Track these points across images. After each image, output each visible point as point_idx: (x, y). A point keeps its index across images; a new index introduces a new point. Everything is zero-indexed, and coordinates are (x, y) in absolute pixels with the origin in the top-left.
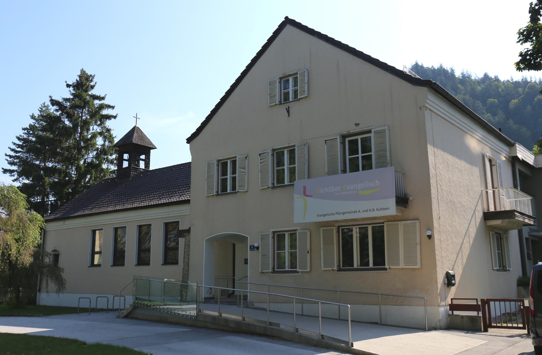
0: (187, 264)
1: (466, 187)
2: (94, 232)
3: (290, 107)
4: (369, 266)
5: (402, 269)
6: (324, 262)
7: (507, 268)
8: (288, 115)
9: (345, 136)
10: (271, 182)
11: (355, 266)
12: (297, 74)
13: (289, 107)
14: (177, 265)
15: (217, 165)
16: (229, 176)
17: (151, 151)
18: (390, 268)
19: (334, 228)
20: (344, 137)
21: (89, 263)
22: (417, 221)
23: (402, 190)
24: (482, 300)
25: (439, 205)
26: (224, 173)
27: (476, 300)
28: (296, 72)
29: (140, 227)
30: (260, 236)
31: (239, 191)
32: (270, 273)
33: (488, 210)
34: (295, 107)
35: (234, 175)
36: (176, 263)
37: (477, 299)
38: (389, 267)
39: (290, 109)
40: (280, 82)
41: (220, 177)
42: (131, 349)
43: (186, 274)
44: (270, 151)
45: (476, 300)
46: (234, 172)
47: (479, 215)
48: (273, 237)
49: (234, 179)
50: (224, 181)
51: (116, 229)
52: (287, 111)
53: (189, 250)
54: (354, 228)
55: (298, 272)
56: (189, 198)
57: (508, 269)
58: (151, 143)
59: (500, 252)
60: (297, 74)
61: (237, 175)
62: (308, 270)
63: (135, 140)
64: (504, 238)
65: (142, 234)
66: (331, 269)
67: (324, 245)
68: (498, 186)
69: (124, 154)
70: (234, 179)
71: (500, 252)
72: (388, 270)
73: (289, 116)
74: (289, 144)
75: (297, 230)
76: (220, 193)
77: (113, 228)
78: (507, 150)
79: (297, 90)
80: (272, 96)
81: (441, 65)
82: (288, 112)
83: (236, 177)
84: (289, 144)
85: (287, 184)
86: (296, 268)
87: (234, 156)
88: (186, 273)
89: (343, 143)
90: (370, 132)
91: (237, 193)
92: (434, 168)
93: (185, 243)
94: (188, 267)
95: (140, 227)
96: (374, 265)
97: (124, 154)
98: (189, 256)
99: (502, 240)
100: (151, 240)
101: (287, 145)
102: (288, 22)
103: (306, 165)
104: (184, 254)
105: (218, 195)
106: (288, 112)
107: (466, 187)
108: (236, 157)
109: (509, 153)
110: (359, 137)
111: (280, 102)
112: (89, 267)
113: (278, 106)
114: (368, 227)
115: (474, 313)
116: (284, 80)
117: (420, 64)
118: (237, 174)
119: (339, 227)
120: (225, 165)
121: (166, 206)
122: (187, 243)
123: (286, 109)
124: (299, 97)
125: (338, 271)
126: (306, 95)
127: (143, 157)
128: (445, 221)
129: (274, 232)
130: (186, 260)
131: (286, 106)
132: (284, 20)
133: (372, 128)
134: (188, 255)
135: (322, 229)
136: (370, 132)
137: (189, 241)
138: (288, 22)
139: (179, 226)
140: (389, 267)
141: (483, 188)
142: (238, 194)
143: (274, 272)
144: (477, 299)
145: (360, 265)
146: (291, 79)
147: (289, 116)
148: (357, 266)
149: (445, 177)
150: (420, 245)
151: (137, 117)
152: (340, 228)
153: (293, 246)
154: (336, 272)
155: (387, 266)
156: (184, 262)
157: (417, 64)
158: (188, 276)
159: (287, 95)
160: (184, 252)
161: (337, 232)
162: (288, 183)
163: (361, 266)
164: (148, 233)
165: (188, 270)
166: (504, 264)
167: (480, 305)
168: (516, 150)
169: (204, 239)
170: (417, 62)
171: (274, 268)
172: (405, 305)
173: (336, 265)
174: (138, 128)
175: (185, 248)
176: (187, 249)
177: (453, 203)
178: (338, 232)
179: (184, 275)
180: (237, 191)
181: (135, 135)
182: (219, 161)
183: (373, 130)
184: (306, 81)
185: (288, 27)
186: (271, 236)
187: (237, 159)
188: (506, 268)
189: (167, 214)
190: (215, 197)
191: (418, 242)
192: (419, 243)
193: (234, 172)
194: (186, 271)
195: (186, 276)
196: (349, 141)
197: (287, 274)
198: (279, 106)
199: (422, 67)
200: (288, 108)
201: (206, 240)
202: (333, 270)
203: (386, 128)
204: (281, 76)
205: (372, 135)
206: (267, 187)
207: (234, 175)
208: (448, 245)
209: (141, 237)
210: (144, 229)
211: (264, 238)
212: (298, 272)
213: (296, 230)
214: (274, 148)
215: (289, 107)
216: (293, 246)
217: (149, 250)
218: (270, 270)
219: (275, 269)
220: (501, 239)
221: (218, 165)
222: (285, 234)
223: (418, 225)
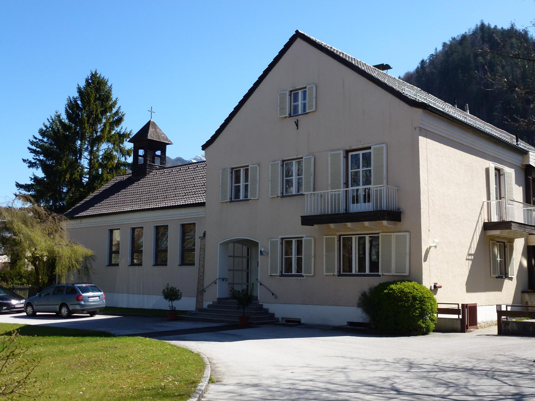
0: (202, 266)
1: (464, 199)
2: (111, 231)
3: (298, 120)
4: (365, 272)
5: (393, 275)
6: (326, 268)
7: (509, 275)
8: (297, 128)
9: (347, 150)
10: (281, 191)
11: (354, 272)
12: (306, 88)
13: (297, 120)
14: (193, 266)
15: (231, 173)
16: (242, 184)
17: (167, 146)
18: (383, 275)
19: (336, 237)
20: (347, 152)
21: (107, 262)
22: (407, 233)
23: (396, 204)
24: (463, 305)
25: (430, 218)
26: (238, 180)
27: (457, 305)
28: (304, 86)
29: (157, 228)
30: (269, 242)
31: (251, 198)
32: (278, 277)
33: (491, 221)
34: (303, 120)
35: (247, 183)
36: (193, 264)
37: (458, 304)
38: (382, 274)
39: (299, 122)
40: (290, 95)
41: (233, 185)
42: (329, 48)
43: (201, 276)
44: (279, 162)
45: (457, 305)
46: (246, 180)
47: (481, 225)
48: (282, 243)
49: (246, 187)
50: (238, 189)
51: (133, 229)
52: (296, 124)
53: (204, 253)
54: (354, 237)
55: (303, 276)
56: (205, 201)
57: (510, 276)
58: (167, 139)
59: (504, 260)
60: (306, 88)
61: (249, 183)
62: (312, 275)
63: (151, 135)
64: (508, 246)
65: (159, 235)
66: (332, 274)
67: (326, 252)
68: (505, 196)
69: (139, 150)
70: (246, 187)
71: (503, 260)
72: (381, 276)
73: (298, 129)
74: (297, 156)
75: (303, 237)
76: (234, 199)
77: (131, 228)
78: (519, 159)
79: (306, 103)
80: (282, 109)
81: (512, 25)
82: (297, 125)
83: (248, 184)
84: (297, 156)
85: (295, 194)
86: (302, 273)
87: (246, 164)
88: (201, 275)
89: (346, 157)
90: (369, 148)
91: (249, 200)
92: (426, 184)
93: (201, 246)
94: (204, 269)
95: (157, 228)
96: (370, 271)
97: (139, 150)
98: (204, 259)
99: (506, 248)
100: (168, 241)
101: (295, 157)
102: (298, 35)
103: (312, 177)
104: (200, 257)
105: (231, 201)
106: (297, 125)
107: (464, 199)
108: (248, 166)
109: (522, 161)
110: (361, 153)
111: (290, 114)
112: (107, 266)
113: (288, 118)
114: (365, 237)
115: (455, 316)
116: (294, 94)
117: (486, 23)
118: (249, 181)
119: (340, 236)
120: (238, 173)
121: (182, 207)
122: (203, 246)
123: (295, 122)
124: (307, 111)
125: (338, 276)
126: (314, 109)
127: (158, 153)
128: (435, 233)
129: (282, 239)
130: (201, 262)
131: (294, 119)
132: (295, 33)
133: (372, 145)
134: (204, 258)
135: (325, 237)
136: (369, 148)
137: (204, 245)
138: (298, 35)
139: (195, 227)
140: (382, 274)
141: (485, 199)
142: (250, 201)
143: (282, 275)
144: (458, 304)
145: (358, 271)
146: (300, 93)
147: (298, 129)
148: (355, 272)
149: (438, 192)
150: (409, 255)
151: (153, 111)
152: (342, 237)
153: (299, 252)
154: (337, 277)
155: (380, 273)
156: (199, 265)
157: (483, 25)
158: (203, 278)
159: (296, 108)
160: (200, 255)
161: (338, 240)
162: (296, 193)
163: (359, 272)
164: (165, 234)
165: (204, 272)
166: (507, 272)
167: (460, 309)
168: (529, 158)
169: (218, 243)
170: (483, 21)
171: (281, 272)
172: (342, 306)
173: (336, 271)
174: (154, 123)
175: (200, 252)
176: (203, 252)
177: (447, 215)
178: (339, 240)
179: (200, 277)
180: (249, 198)
181: (151, 130)
182: (232, 169)
183: (372, 147)
184: (314, 96)
185: (299, 41)
186: (279, 242)
187: (249, 168)
188: (508, 276)
189: (184, 215)
190: (229, 203)
191: (407, 252)
192: (408, 253)
193: (246, 180)
194: (202, 272)
195: (201, 278)
196: (352, 155)
197: (293, 278)
198: (289, 118)
199: (489, 28)
200: (296, 121)
201: (220, 244)
202: (334, 275)
203: (384, 145)
204: (291, 89)
205: (371, 151)
206: (276, 196)
207: (247, 183)
208: (438, 255)
209: (159, 237)
210: (161, 230)
211: (273, 244)
212: (303, 276)
213: (302, 237)
214: (284, 159)
215: (297, 120)
216: (299, 252)
217: (166, 251)
218: (278, 274)
219: (282, 273)
220: (505, 247)
221: (231, 173)
222: (292, 240)
223: (408, 237)
